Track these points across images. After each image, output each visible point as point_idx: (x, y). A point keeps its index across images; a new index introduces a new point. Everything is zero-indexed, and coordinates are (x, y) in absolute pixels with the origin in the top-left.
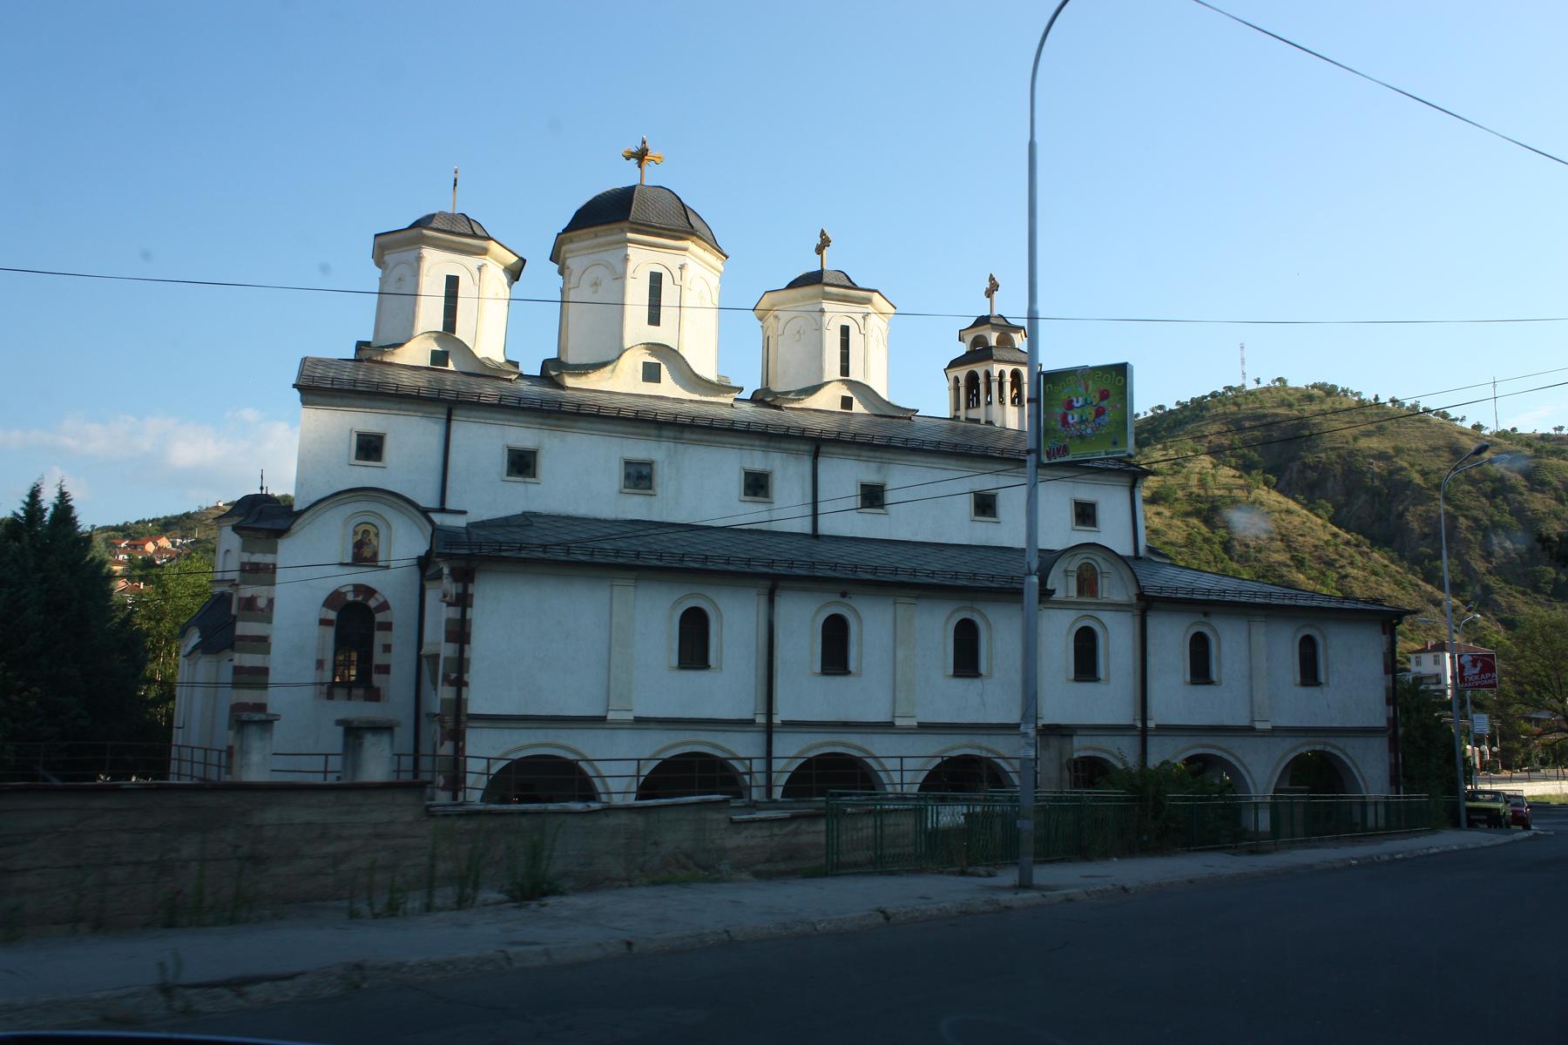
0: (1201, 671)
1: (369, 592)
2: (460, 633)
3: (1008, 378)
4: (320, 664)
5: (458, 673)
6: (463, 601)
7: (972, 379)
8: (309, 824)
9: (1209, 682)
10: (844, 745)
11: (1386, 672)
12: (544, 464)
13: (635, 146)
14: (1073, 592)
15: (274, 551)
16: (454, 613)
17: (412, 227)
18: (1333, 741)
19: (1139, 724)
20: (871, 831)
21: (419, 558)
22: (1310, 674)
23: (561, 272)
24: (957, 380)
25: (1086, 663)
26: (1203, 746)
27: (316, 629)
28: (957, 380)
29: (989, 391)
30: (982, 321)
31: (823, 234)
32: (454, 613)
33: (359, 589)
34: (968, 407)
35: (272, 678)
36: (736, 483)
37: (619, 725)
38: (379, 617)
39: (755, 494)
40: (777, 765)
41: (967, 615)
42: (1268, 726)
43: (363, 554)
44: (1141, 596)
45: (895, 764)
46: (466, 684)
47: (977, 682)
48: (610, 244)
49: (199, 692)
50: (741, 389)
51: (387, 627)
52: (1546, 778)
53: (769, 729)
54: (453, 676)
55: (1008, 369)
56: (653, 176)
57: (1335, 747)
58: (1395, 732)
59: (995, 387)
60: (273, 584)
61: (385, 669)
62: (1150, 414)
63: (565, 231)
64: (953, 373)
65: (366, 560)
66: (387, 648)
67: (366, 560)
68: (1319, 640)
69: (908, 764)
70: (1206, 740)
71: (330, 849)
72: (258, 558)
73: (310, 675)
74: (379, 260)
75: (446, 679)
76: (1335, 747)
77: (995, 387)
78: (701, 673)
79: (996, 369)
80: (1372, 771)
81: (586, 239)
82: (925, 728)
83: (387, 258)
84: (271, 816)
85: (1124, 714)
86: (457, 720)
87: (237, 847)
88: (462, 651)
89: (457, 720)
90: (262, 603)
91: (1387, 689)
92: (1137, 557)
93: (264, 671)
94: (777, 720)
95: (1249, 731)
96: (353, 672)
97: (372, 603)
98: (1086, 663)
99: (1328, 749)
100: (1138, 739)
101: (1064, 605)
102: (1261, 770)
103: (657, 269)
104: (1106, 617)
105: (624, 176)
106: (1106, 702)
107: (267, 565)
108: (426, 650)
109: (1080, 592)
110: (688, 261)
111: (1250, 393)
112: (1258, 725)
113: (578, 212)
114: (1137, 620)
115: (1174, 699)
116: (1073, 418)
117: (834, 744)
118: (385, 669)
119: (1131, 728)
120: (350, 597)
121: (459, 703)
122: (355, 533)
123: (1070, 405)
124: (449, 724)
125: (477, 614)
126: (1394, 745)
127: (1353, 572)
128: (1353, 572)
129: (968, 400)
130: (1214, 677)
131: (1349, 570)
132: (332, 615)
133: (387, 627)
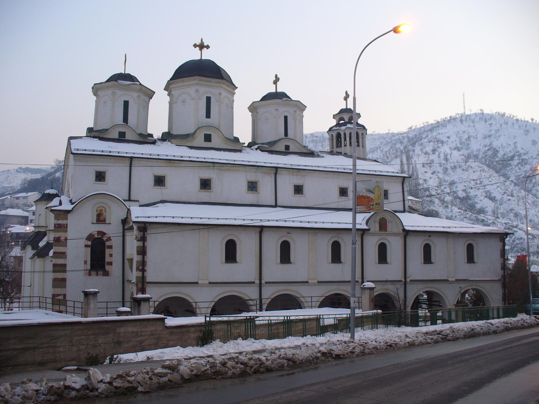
0: (427, 259)
1: (104, 234)
2: (142, 251)
4: (85, 262)
5: (142, 266)
6: (143, 239)
7: (339, 135)
8: (133, 332)
10: (289, 290)
11: (501, 257)
12: (168, 181)
13: (198, 42)
14: (377, 228)
15: (67, 219)
16: (140, 244)
18: (479, 284)
19: (403, 280)
20: (302, 327)
21: (122, 220)
22: (470, 259)
23: (169, 95)
24: (332, 136)
25: (383, 257)
26: (428, 288)
27: (83, 249)
28: (332, 136)
29: (345, 140)
30: (342, 111)
31: (276, 76)
32: (140, 244)
33: (99, 233)
34: (337, 147)
35: (68, 268)
36: (244, 186)
38: (107, 244)
39: (252, 190)
40: (263, 301)
41: (336, 239)
43: (100, 219)
45: (309, 299)
46: (146, 271)
47: (341, 265)
48: (190, 85)
49: (37, 275)
50: (244, 143)
51: (110, 247)
54: (141, 268)
56: (207, 55)
57: (481, 287)
58: (505, 280)
59: (348, 139)
60: (66, 231)
61: (110, 264)
62: (422, 125)
63: (171, 79)
64: (331, 133)
65: (101, 221)
66: (111, 255)
67: (101, 221)
68: (475, 245)
69: (314, 299)
70: (429, 285)
71: (139, 339)
72: (60, 222)
73: (82, 266)
74: (95, 94)
75: (138, 269)
76: (481, 287)
77: (348, 139)
78: (234, 264)
80: (495, 297)
81: (180, 83)
83: (99, 93)
84: (122, 330)
85: (399, 276)
86: (143, 285)
87: (113, 339)
88: (143, 258)
89: (143, 285)
90: (63, 239)
91: (501, 264)
93: (65, 265)
97: (105, 239)
98: (383, 257)
99: (478, 288)
101: (374, 234)
102: (450, 297)
103: (209, 95)
104: (390, 238)
105: (195, 55)
106: (392, 270)
107: (64, 224)
108: (127, 256)
109: (381, 229)
110: (221, 91)
111: (467, 116)
112: (450, 279)
113: (177, 70)
114: (403, 239)
115: (418, 269)
117: (286, 290)
118: (110, 264)
120: (96, 237)
121: (143, 277)
122: (97, 211)
124: (140, 286)
125: (148, 244)
126: (504, 286)
129: (337, 143)
130: (433, 261)
132: (89, 243)
133: (110, 247)
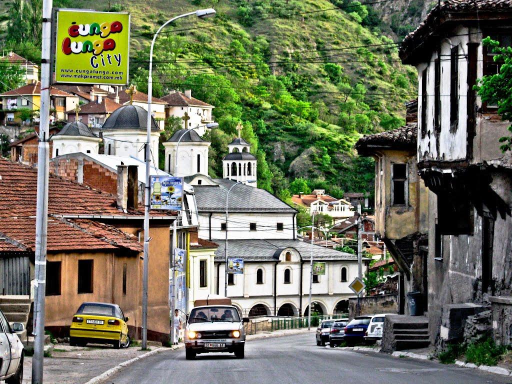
0: (315, 279)
3: (247, 166)
9: (318, 282)
17: (264, 240)
37: (247, 298)
42: (332, 294)
44: (301, 260)
52: (109, 131)
53: (275, 297)
55: (247, 162)
79: (242, 163)
82: (251, 297)
92: (294, 239)
94: (303, 294)
95: (327, 295)
96: (364, 291)
100: (299, 299)
104: (293, 266)
112: (330, 294)
116: (77, 45)
119: (272, 296)
123: (74, 31)
127: (383, 84)
128: (383, 84)
130: (319, 281)
131: (378, 82)
